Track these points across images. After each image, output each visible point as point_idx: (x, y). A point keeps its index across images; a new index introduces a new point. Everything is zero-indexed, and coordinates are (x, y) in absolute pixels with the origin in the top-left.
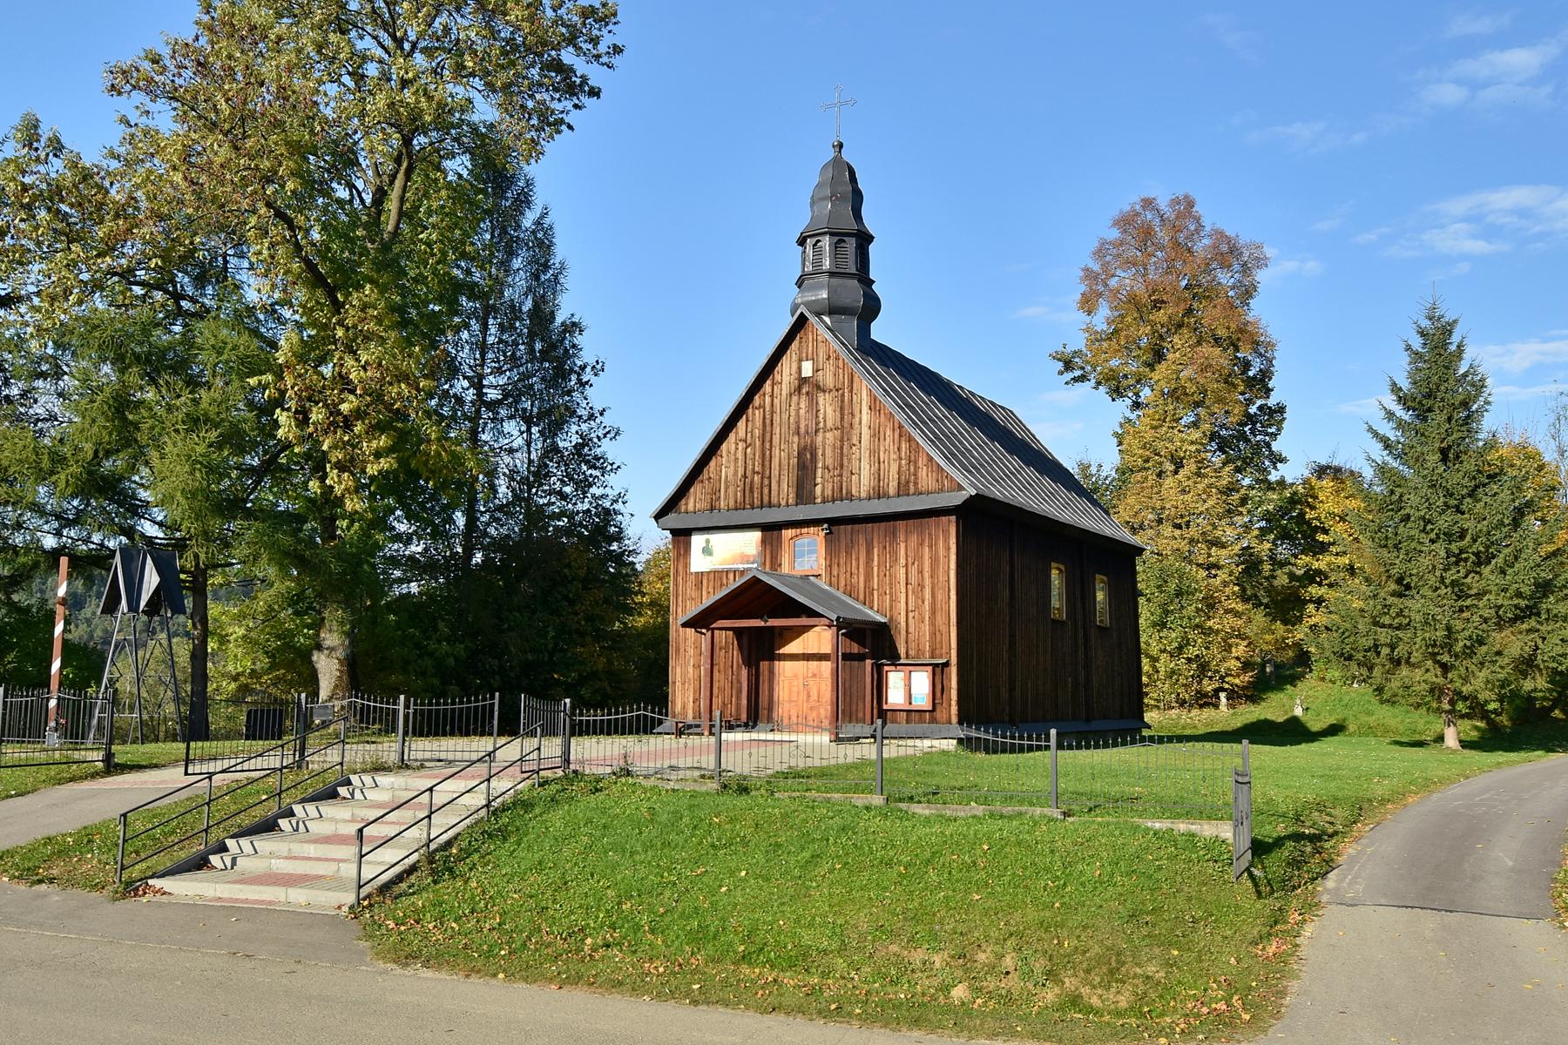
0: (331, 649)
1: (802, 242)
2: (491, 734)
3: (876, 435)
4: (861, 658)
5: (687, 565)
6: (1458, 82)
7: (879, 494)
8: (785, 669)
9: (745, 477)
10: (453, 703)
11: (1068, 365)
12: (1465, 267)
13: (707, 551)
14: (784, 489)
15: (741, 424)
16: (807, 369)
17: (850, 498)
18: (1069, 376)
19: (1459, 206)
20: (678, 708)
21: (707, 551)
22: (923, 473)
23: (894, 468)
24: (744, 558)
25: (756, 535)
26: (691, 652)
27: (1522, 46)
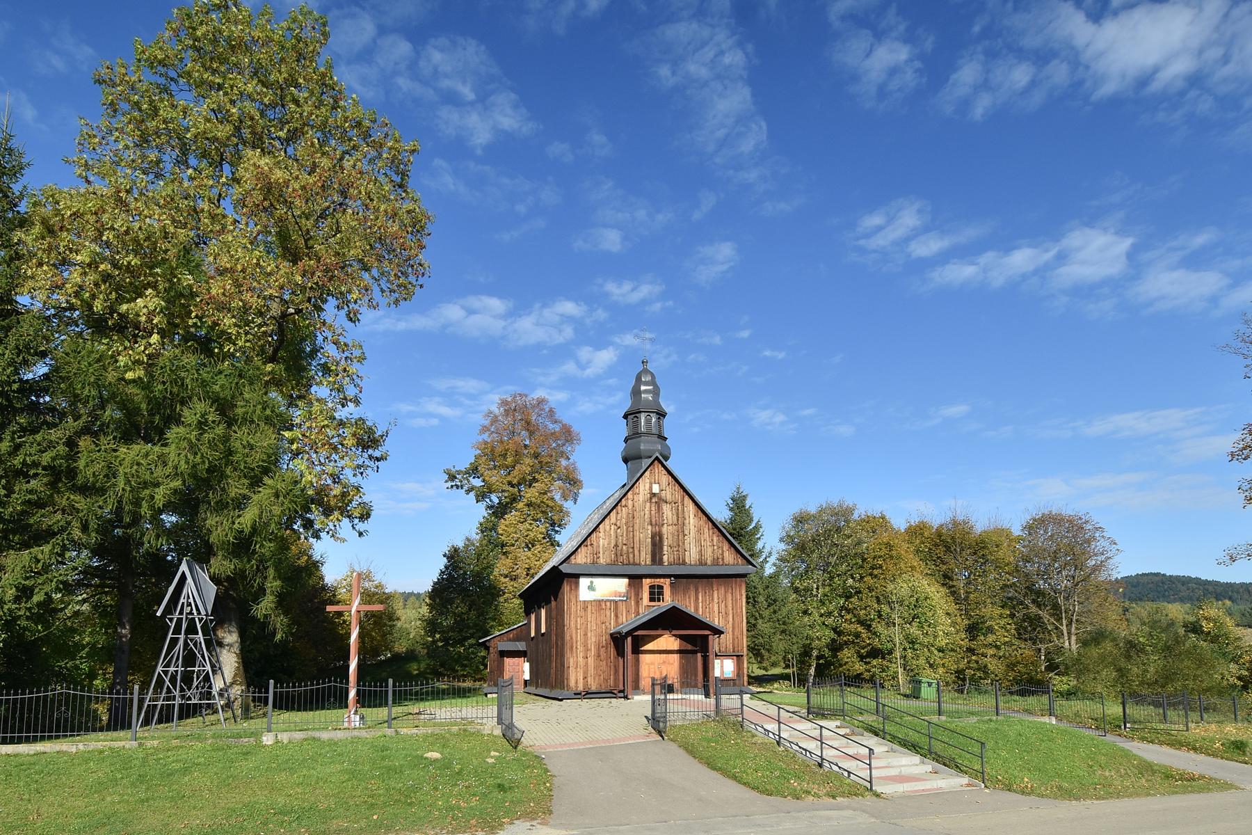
0: (230, 645)
1: (625, 417)
2: (386, 705)
3: (699, 531)
4: (695, 652)
5: (577, 596)
6: (463, 307)
7: (702, 563)
8: (645, 659)
9: (616, 545)
10: (294, 686)
11: (452, 477)
12: (435, 422)
13: (591, 588)
14: (645, 557)
15: (613, 514)
16: (656, 489)
17: (684, 563)
18: (449, 484)
19: (442, 384)
20: (572, 683)
21: (591, 588)
22: (726, 554)
23: (710, 550)
24: (616, 594)
25: (626, 581)
26: (580, 648)
27: (500, 297)
